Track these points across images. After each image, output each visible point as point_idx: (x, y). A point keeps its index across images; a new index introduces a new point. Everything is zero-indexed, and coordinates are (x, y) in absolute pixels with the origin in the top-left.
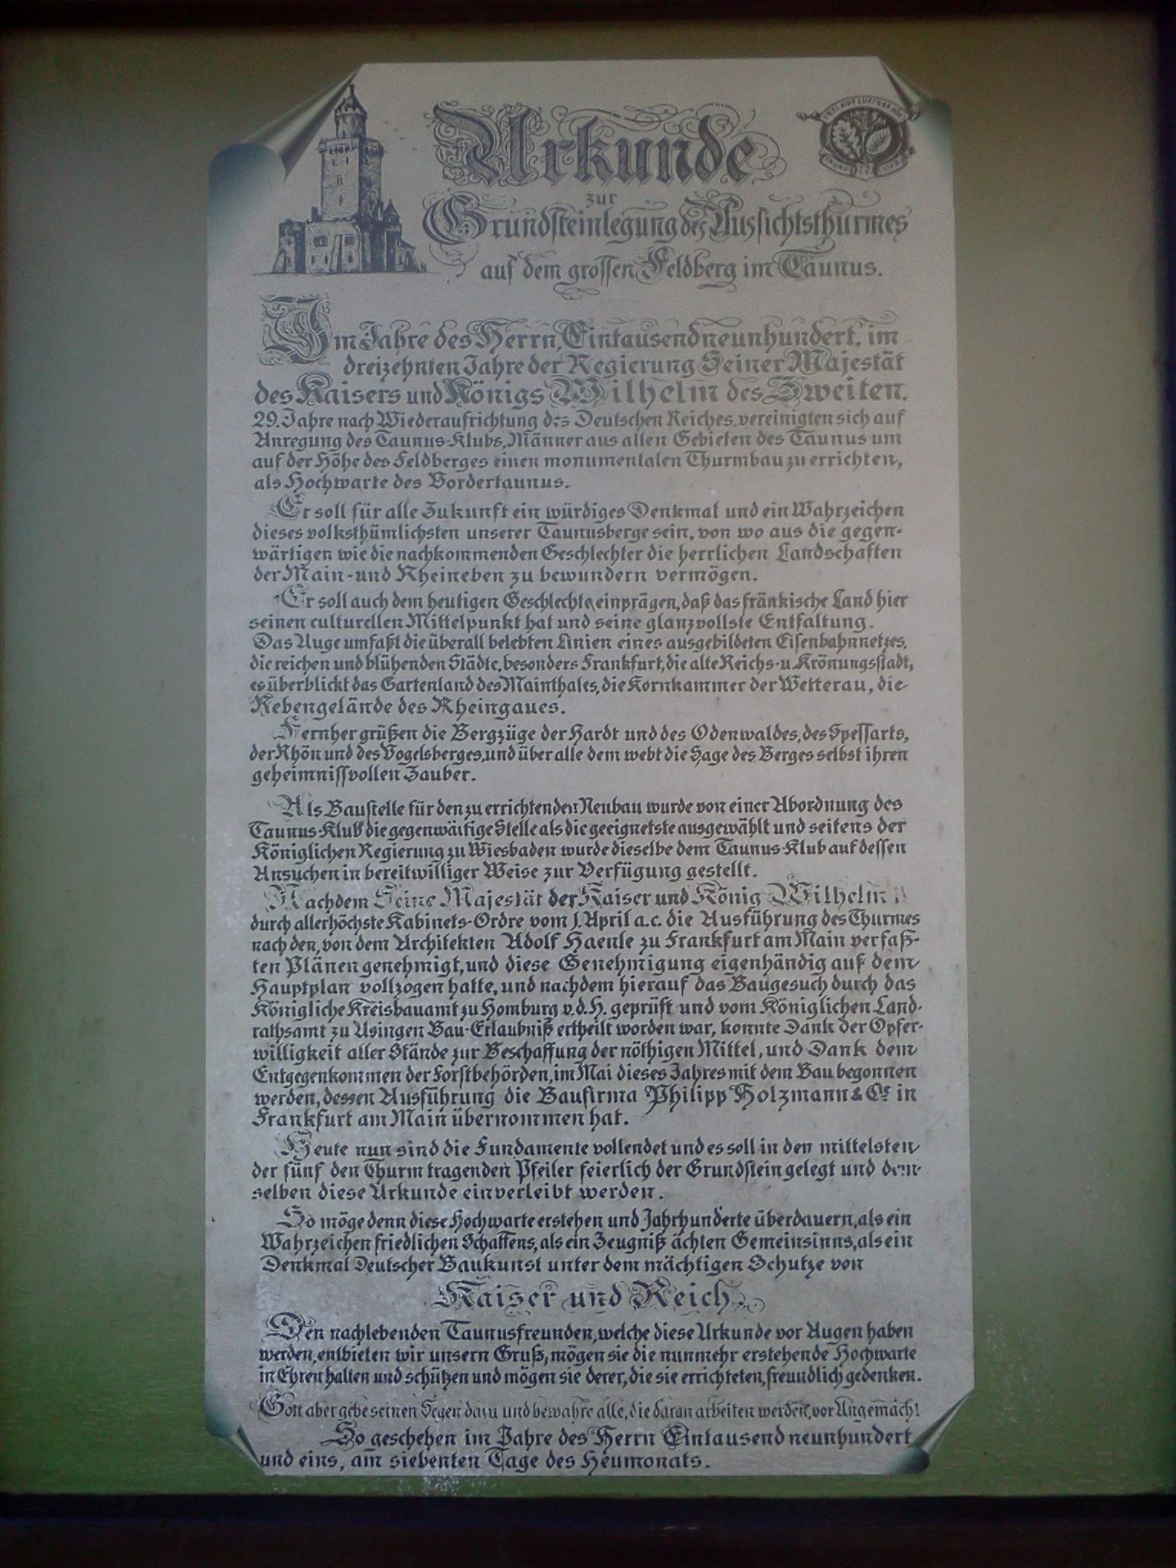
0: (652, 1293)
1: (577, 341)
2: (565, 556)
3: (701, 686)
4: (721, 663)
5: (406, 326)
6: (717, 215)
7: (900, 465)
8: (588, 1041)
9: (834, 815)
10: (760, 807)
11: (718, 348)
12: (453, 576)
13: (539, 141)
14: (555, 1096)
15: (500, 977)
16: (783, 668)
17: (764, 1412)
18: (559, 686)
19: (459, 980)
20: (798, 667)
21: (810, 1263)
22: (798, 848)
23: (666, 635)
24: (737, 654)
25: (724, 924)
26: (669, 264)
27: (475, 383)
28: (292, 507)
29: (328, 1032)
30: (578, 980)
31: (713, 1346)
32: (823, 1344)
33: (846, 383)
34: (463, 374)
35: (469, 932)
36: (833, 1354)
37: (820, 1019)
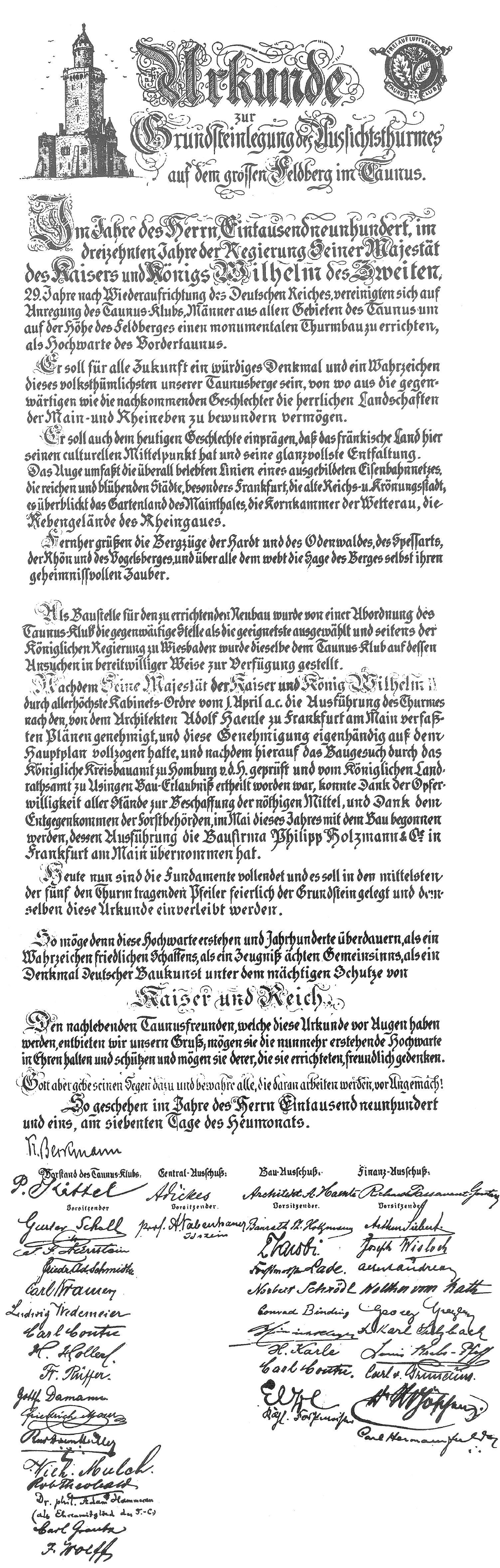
0: (273, 995)
1: (231, 232)
2: (224, 403)
3: (311, 505)
4: (324, 487)
5: (121, 220)
6: (319, 130)
7: (437, 330)
8: (235, 795)
9: (391, 622)
10: (345, 616)
11: (321, 237)
12: (153, 419)
13: (204, 70)
14: (214, 836)
15: (180, 746)
16: (363, 490)
17: (345, 1086)
18: (221, 505)
19: (155, 748)
20: (373, 489)
21: (374, 972)
22: (369, 647)
23: (287, 464)
24: (334, 479)
25: (321, 706)
26: (288, 170)
27: (166, 265)
28: (50, 364)
29: (73, 787)
30: (230, 748)
31: (311, 1035)
32: (382, 1034)
33: (402, 266)
34: (158, 258)
35: (161, 711)
36: (388, 1041)
37: (380, 779)
